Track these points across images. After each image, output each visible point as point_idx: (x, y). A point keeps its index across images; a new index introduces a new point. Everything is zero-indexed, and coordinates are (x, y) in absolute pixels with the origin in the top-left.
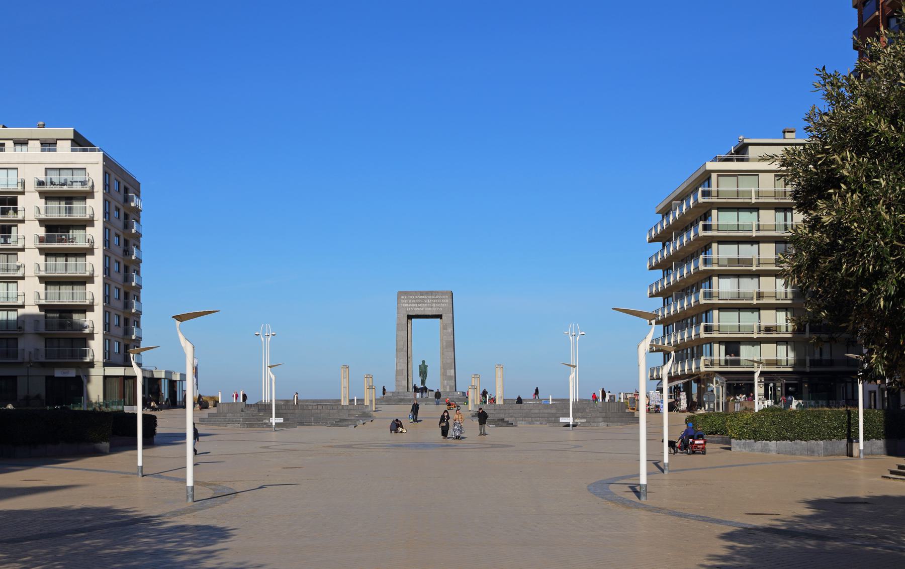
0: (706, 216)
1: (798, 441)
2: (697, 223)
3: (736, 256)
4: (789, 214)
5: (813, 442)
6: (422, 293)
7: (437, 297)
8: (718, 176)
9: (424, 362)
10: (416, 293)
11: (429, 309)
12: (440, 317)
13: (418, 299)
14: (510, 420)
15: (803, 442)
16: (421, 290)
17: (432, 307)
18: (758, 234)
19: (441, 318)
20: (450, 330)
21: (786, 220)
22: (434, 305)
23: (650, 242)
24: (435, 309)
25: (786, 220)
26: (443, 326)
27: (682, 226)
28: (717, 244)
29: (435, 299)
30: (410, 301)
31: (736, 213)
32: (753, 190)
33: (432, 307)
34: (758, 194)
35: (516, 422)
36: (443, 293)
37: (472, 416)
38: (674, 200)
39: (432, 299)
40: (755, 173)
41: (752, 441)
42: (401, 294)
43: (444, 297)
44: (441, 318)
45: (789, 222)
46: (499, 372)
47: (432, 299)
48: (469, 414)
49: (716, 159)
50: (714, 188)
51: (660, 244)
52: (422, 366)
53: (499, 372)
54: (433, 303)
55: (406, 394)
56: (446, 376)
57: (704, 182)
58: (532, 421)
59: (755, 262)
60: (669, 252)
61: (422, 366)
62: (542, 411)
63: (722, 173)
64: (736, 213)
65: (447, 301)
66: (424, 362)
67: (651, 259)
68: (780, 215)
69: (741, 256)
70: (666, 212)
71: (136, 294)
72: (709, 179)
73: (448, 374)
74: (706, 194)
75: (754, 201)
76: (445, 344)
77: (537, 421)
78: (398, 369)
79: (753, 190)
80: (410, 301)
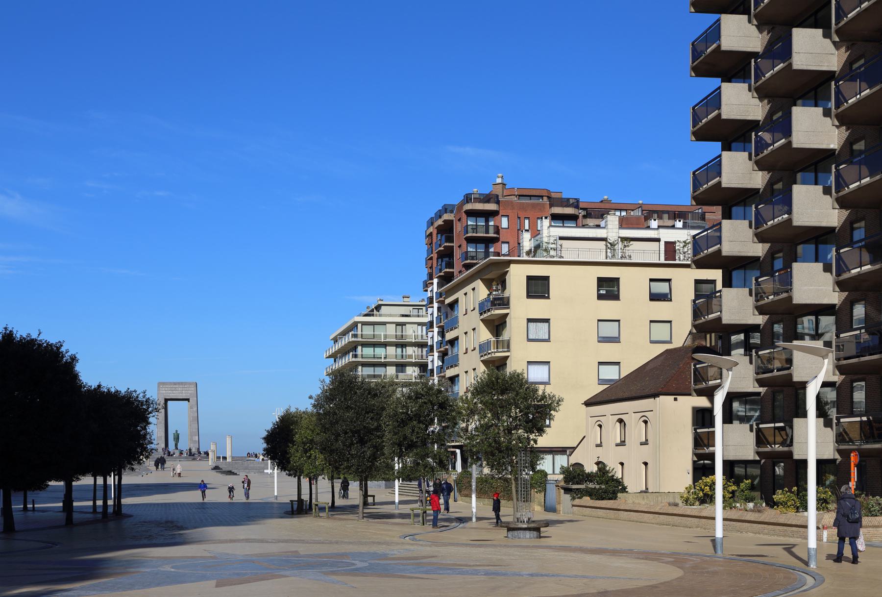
0: (355, 349)
1: (374, 481)
2: (349, 353)
3: (373, 373)
4: (404, 349)
5: (380, 482)
6: (175, 384)
7: (186, 386)
8: (362, 325)
9: (177, 431)
10: (170, 383)
11: (181, 394)
12: (188, 400)
13: (172, 387)
14: (235, 471)
15: (376, 482)
16: (175, 381)
17: (182, 393)
18: (385, 360)
19: (189, 401)
20: (195, 409)
21: (402, 352)
22: (184, 392)
23: (327, 358)
24: (184, 394)
25: (402, 352)
26: (190, 407)
27: (343, 352)
28: (395, 347)
29: (185, 387)
30: (166, 389)
31: (373, 348)
32: (382, 334)
33: (182, 393)
34: (386, 336)
35: (239, 472)
36: (190, 384)
37: (212, 469)
38: (338, 335)
39: (182, 388)
40: (384, 324)
41: (353, 481)
42: (160, 384)
43: (191, 386)
44: (189, 401)
45: (404, 353)
46: (228, 440)
47: (182, 388)
48: (210, 468)
49: (360, 315)
50: (359, 332)
51: (333, 359)
52: (176, 434)
53: (228, 440)
54: (183, 390)
55: (248, 473)
56: (192, 440)
57: (354, 327)
58: (249, 472)
59: (538, 308)
60: (339, 366)
61: (176, 434)
62: (255, 466)
63: (364, 324)
64: (373, 348)
65: (193, 389)
66: (177, 431)
67: (327, 368)
68: (399, 350)
69: (376, 373)
70: (335, 340)
71: (362, 516)
72: (357, 326)
73: (194, 440)
74: (355, 336)
75: (382, 340)
76: (191, 419)
77: (252, 472)
78: (159, 435)
79: (382, 334)
80: (166, 389)
